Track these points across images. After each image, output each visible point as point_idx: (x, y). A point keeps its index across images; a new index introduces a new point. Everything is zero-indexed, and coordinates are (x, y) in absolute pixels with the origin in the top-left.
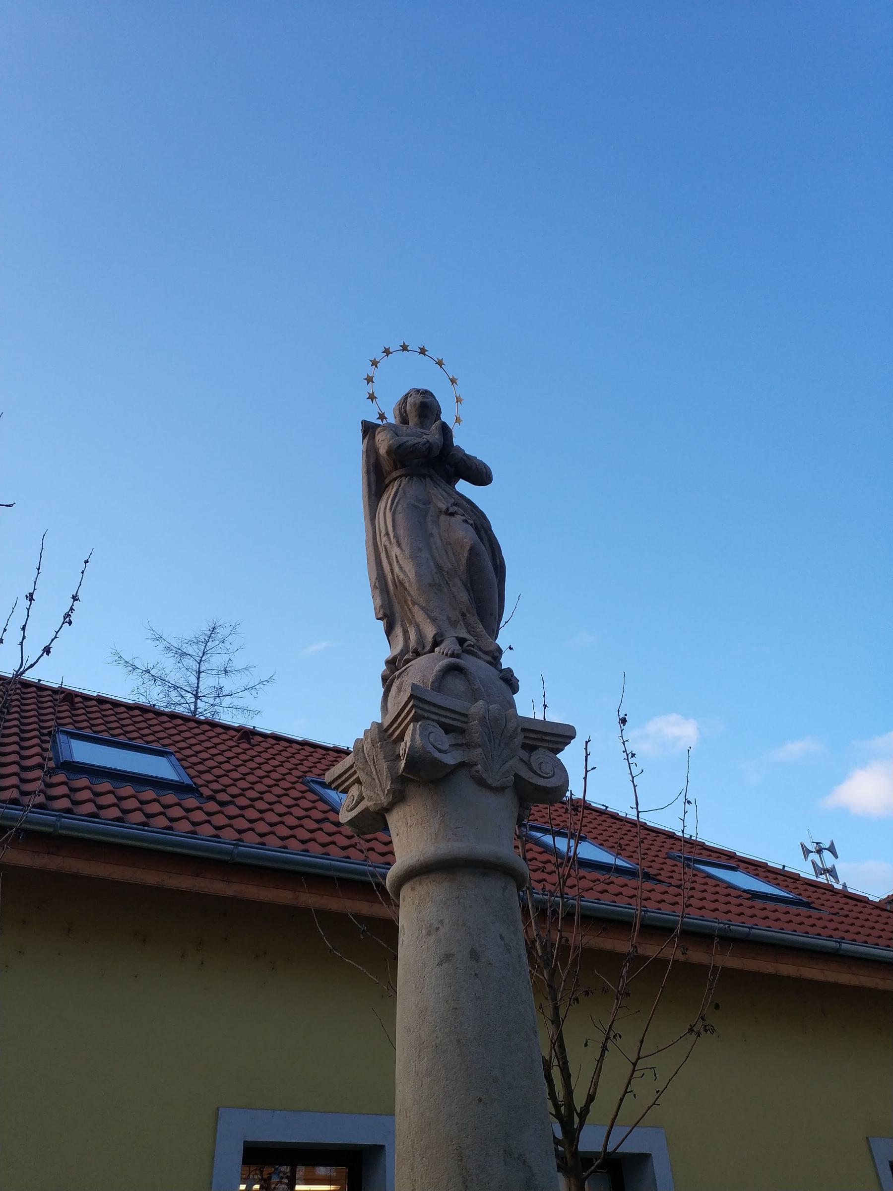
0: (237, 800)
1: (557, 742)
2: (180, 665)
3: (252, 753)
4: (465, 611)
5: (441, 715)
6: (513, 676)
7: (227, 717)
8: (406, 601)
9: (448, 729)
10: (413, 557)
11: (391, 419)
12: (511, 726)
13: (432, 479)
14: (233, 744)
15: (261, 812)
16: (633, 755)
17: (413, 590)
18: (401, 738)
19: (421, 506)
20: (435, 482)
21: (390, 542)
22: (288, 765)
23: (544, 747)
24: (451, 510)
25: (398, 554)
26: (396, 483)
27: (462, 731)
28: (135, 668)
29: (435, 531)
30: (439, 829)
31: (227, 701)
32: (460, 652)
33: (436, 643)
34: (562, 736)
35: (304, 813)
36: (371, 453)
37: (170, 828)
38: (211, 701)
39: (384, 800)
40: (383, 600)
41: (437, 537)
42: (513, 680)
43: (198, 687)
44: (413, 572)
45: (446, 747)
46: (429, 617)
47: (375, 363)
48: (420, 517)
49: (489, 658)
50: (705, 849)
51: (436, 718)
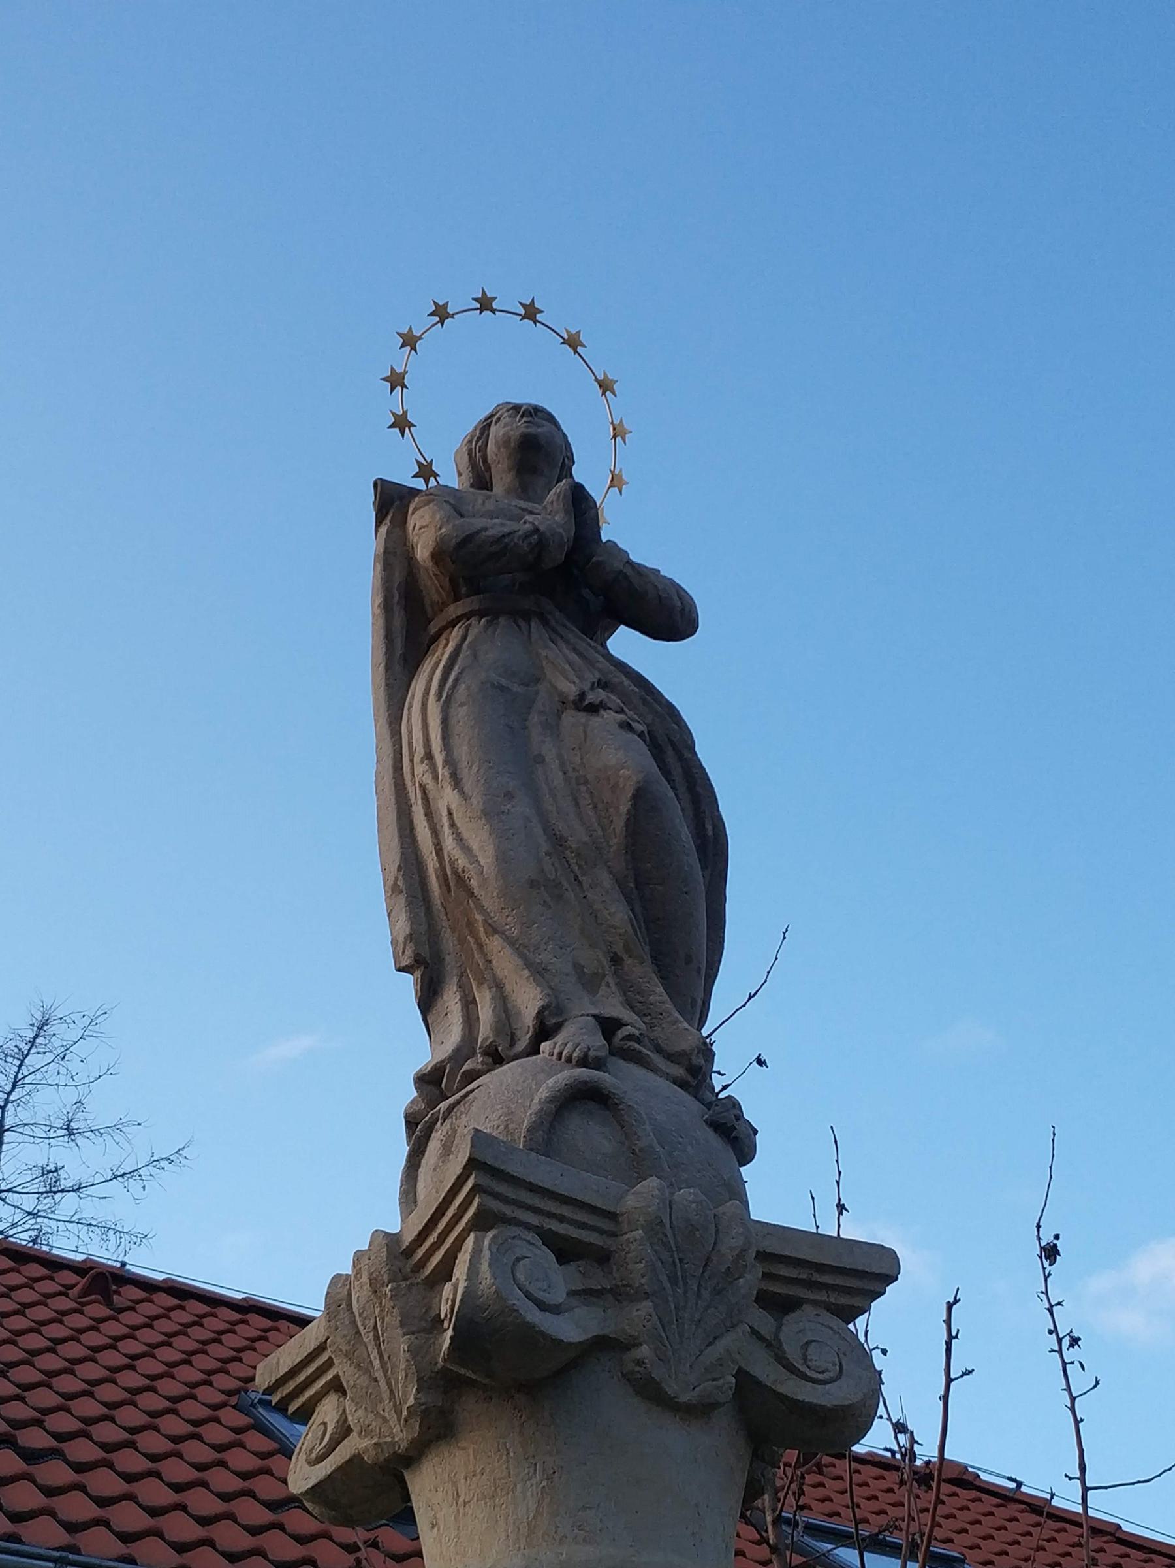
0: (67, 1448)
1: (848, 1291)
3: (113, 1328)
4: (619, 948)
5: (550, 1215)
6: (739, 1116)
7: (67, 1244)
8: (470, 924)
9: (565, 1252)
10: (489, 814)
11: (450, 476)
12: (731, 1243)
13: (545, 622)
14: (69, 1304)
15: (129, 1478)
16: (1075, 1341)
17: (489, 895)
18: (445, 1272)
19: (516, 688)
20: (555, 631)
21: (436, 778)
22: (204, 1362)
23: (815, 1303)
24: (591, 697)
25: (453, 807)
26: (456, 633)
27: (603, 1258)
29: (549, 750)
30: (538, 1513)
31: (68, 1204)
32: (603, 1053)
33: (544, 1032)
34: (864, 1275)
35: (237, 1484)
36: (396, 559)
37: (14, 1538)
38: (29, 1203)
39: (401, 1435)
40: (413, 920)
41: (554, 765)
42: (740, 1126)
44: (490, 850)
45: (558, 1296)
46: (528, 964)
47: (410, 341)
48: (513, 718)
49: (679, 1071)
51: (533, 1219)
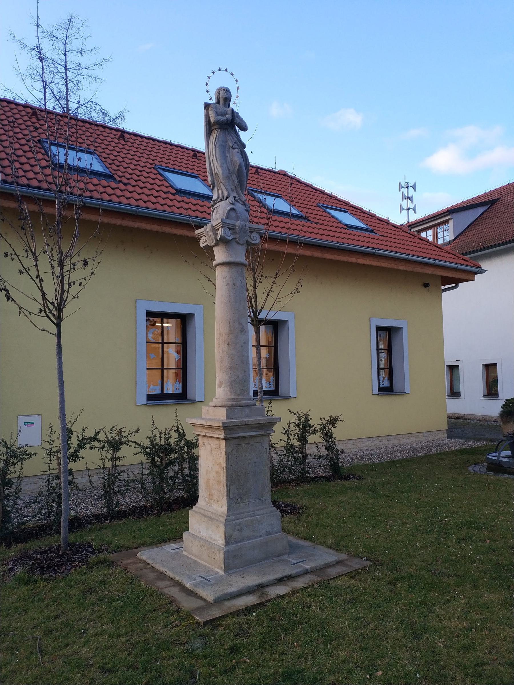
2: (54, 47)
9: (230, 229)
13: (228, 132)
28: (25, 46)
31: (84, 72)
43: (66, 62)
50: (337, 200)
